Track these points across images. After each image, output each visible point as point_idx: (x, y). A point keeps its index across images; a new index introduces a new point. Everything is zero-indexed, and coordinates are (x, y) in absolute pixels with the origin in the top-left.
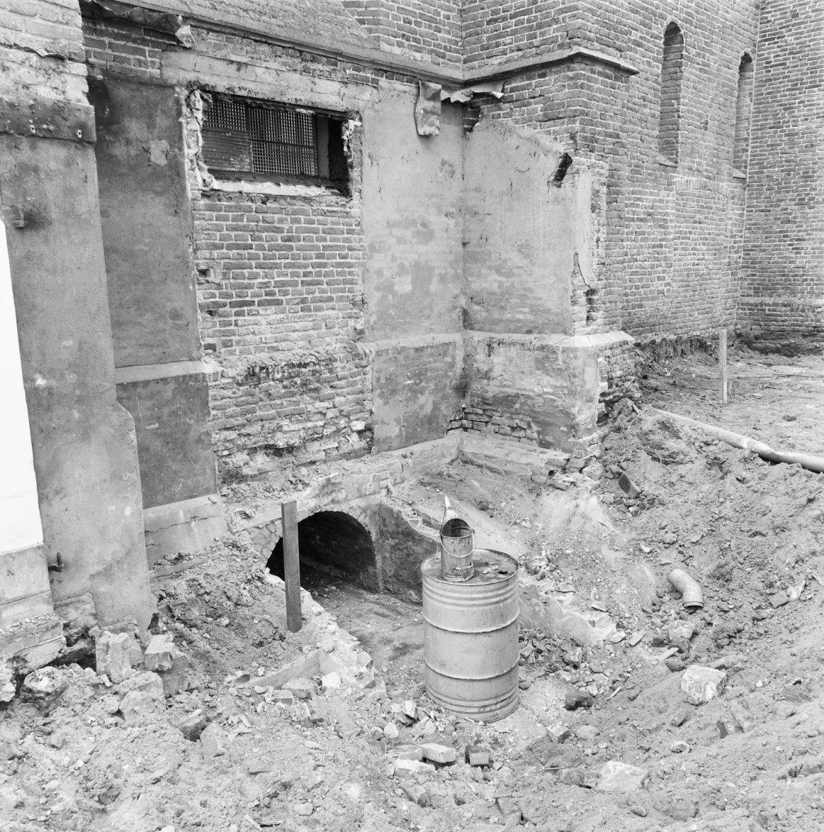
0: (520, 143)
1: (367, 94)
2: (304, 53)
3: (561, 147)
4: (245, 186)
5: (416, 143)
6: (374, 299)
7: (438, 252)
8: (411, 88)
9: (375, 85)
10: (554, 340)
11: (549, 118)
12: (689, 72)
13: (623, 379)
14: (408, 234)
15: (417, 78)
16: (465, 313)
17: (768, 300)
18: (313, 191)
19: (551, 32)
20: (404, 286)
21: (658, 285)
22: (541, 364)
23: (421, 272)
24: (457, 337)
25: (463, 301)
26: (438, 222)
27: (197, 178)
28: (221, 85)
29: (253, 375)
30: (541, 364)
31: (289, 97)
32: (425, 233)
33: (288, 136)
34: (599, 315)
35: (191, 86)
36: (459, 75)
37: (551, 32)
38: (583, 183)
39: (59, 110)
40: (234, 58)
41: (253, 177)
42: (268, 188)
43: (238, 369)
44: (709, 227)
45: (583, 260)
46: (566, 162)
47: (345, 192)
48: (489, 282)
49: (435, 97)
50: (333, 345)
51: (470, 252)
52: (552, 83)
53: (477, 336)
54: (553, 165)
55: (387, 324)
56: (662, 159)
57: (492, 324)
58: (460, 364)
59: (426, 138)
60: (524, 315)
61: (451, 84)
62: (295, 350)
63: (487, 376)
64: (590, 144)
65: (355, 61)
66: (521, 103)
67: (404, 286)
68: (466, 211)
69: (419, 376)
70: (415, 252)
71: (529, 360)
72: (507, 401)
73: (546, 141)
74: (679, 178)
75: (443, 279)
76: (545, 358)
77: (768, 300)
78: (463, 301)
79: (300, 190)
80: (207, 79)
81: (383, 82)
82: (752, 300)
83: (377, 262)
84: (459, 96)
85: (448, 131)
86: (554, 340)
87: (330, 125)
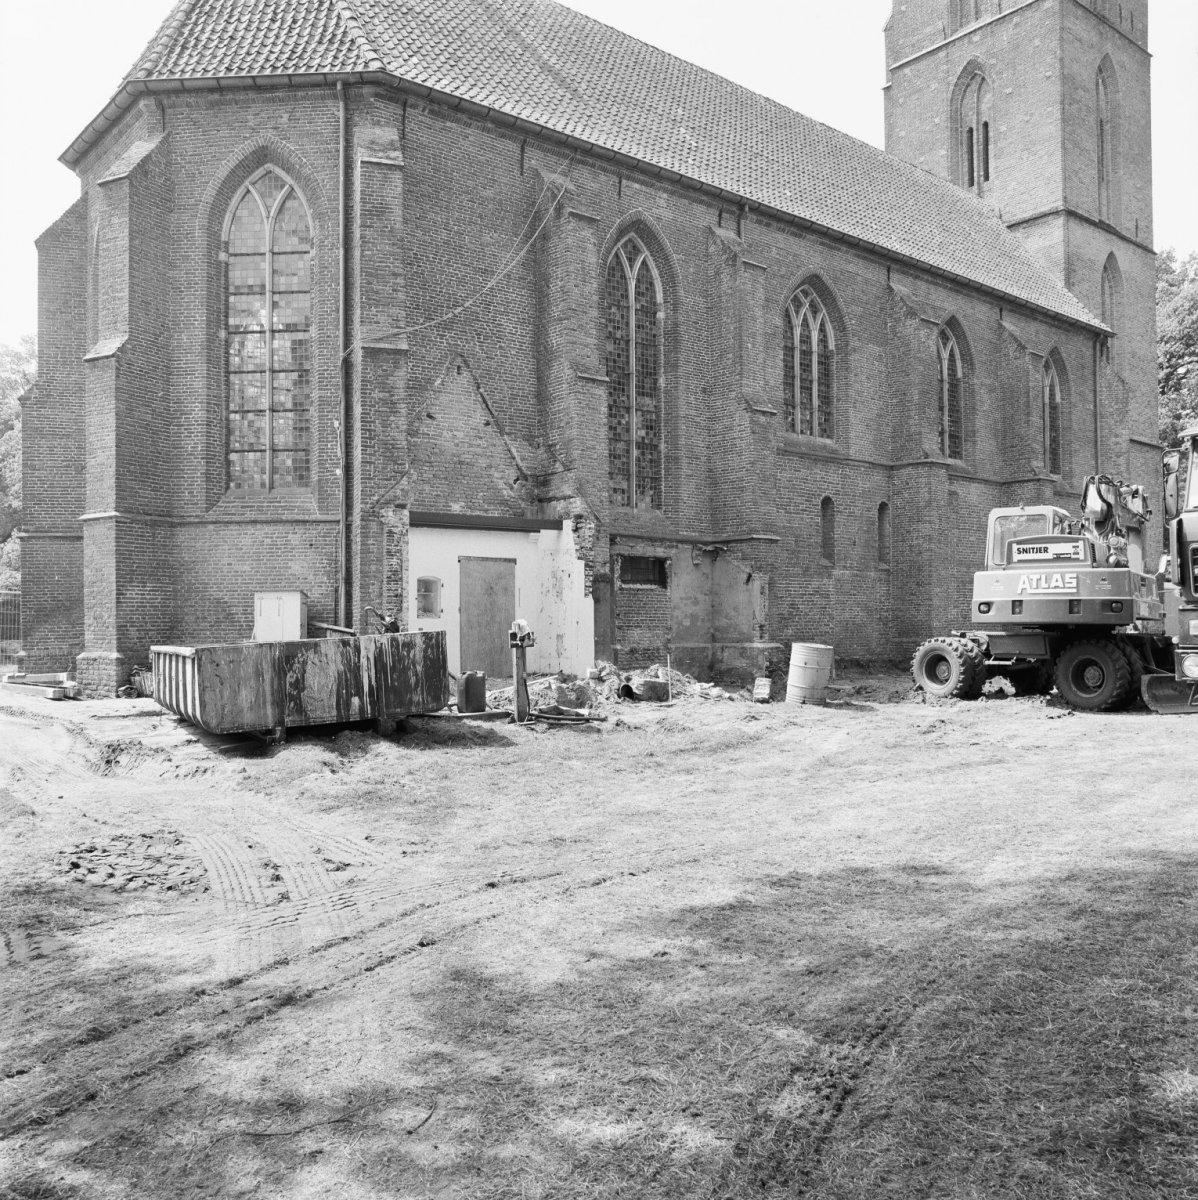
0: (735, 567)
1: (674, 551)
2: (652, 540)
3: (748, 570)
4: (631, 586)
5: (692, 567)
6: (675, 627)
7: (700, 610)
8: (690, 547)
9: (677, 547)
10: (747, 645)
11: (744, 559)
12: (838, 518)
13: (779, 662)
14: (689, 602)
15: (694, 543)
16: (713, 635)
17: (905, 640)
18: (653, 587)
19: (744, 528)
20: (687, 623)
21: (824, 629)
22: (741, 655)
23: (694, 617)
24: (709, 645)
25: (712, 631)
26: (701, 597)
27: (618, 584)
28: (626, 554)
29: (633, 651)
30: (741, 655)
31: (647, 555)
32: (696, 602)
33: (643, 566)
34: (766, 636)
35: (618, 555)
36: (710, 539)
37: (744, 528)
38: (756, 585)
39: (605, 575)
40: (514, 450)
41: (634, 582)
42: (639, 586)
43: (627, 649)
44: (861, 598)
45: (757, 613)
46: (750, 576)
47: (666, 588)
48: (723, 622)
49: (700, 549)
50: (659, 644)
51: (715, 610)
52: (744, 546)
53: (717, 645)
54: (745, 576)
55: (680, 637)
56: (825, 562)
57: (724, 640)
58: (710, 657)
59: (696, 565)
60: (735, 635)
61: (706, 543)
62: (645, 644)
63: (722, 661)
64: (760, 569)
65: (670, 540)
66: (733, 552)
67: (687, 623)
68: (713, 593)
69: (692, 659)
70: (691, 609)
71: (737, 654)
72: (729, 671)
73: (743, 568)
74: (836, 572)
75: (703, 620)
76: (743, 652)
77: (905, 640)
78: (712, 631)
79: (648, 586)
80: (622, 552)
81: (680, 546)
82: (897, 640)
83: (676, 613)
84: (710, 548)
85: (706, 567)
86: (747, 645)
87: (660, 563)
